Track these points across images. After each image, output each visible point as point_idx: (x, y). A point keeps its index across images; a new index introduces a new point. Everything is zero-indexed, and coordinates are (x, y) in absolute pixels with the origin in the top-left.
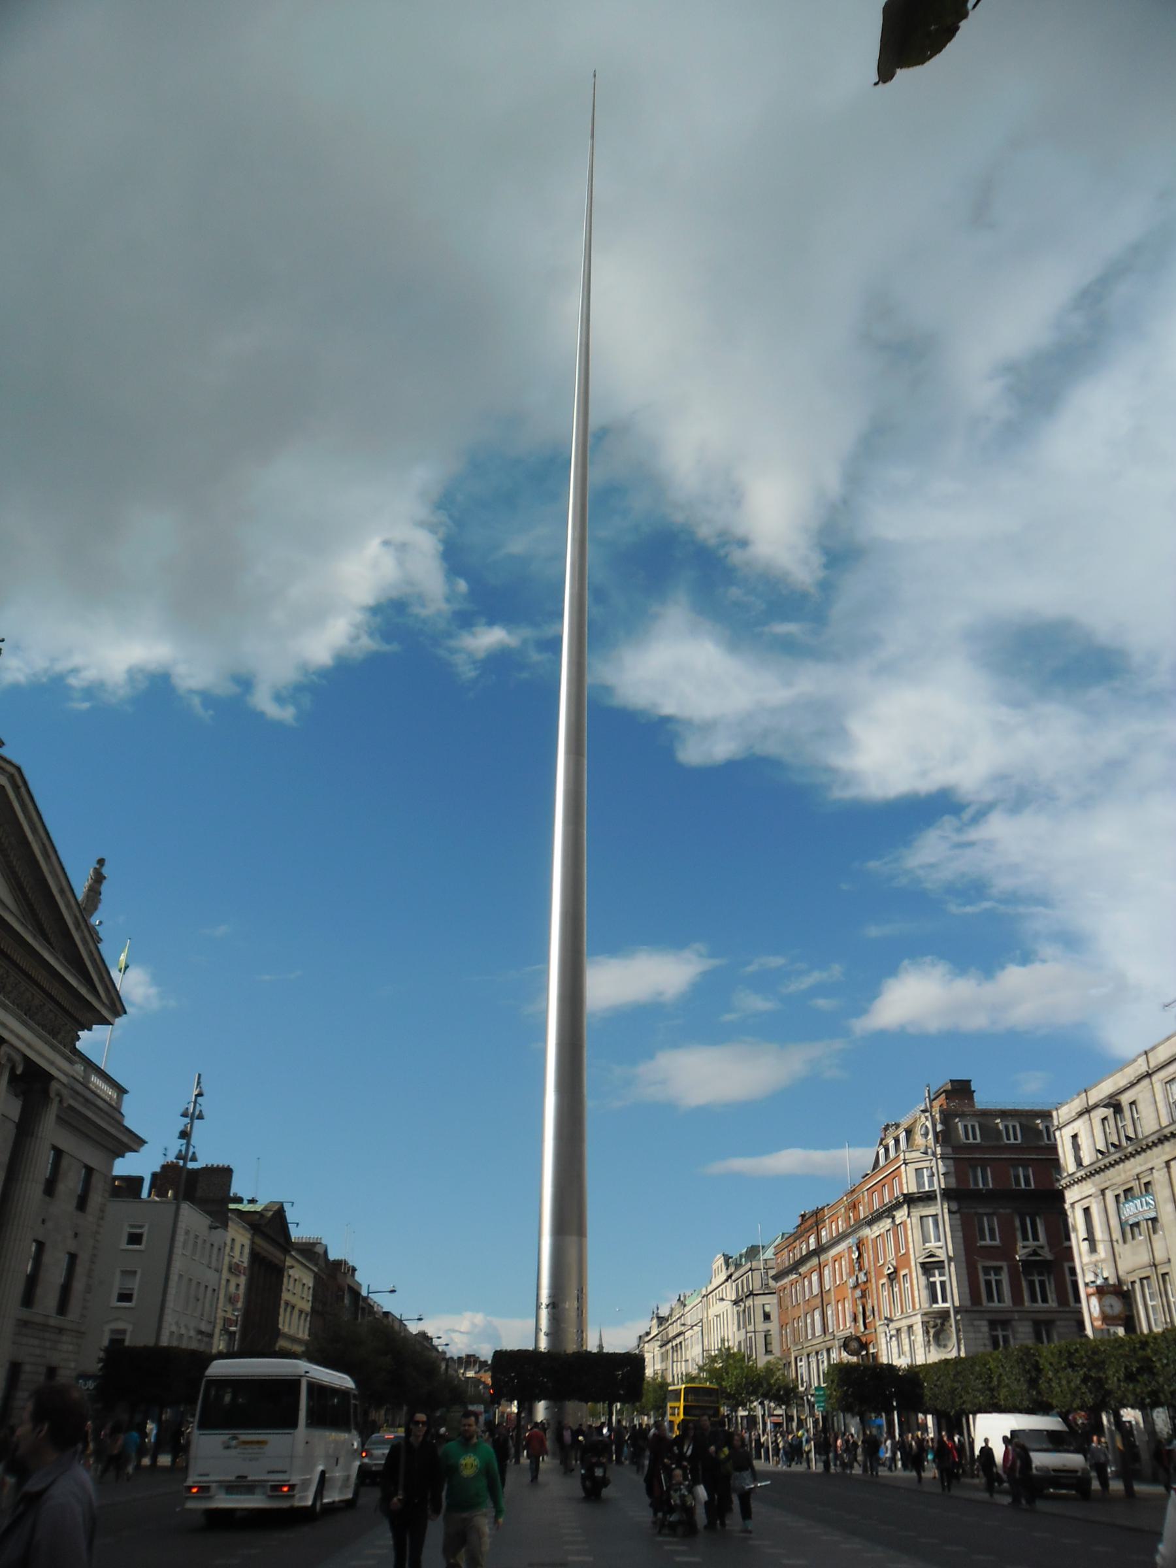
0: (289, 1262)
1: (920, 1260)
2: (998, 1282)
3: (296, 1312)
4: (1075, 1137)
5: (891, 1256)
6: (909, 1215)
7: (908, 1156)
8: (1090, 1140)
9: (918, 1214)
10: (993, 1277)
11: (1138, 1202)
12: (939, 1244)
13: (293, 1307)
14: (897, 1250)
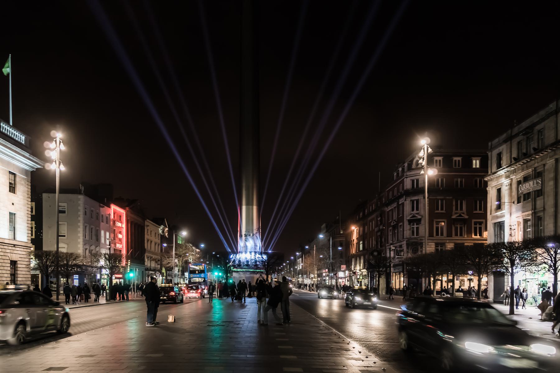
0: (146, 223)
1: (408, 218)
3: (153, 244)
5: (395, 217)
6: (405, 200)
7: (408, 173)
8: (509, 155)
9: (409, 199)
10: (478, 226)
11: (531, 183)
12: (418, 212)
13: (151, 242)
14: (398, 214)
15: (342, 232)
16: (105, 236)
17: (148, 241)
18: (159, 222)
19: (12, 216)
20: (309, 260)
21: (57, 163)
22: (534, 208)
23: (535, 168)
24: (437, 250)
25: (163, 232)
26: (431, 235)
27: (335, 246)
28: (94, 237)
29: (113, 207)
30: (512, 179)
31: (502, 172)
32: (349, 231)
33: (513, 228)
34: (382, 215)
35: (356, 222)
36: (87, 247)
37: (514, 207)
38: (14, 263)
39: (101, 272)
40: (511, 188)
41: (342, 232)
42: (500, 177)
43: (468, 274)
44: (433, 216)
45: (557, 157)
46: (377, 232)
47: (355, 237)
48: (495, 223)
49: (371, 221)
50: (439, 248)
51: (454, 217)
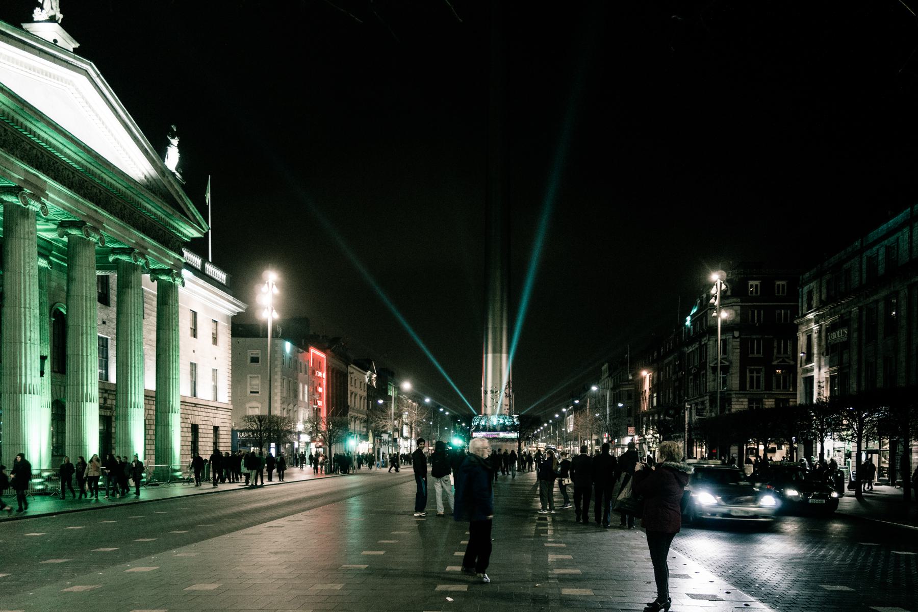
0: (350, 369)
2: (758, 378)
3: (358, 397)
4: (810, 293)
14: (700, 359)
15: (630, 378)
16: (304, 391)
18: (365, 367)
19: (215, 371)
20: (581, 420)
21: (270, 309)
22: (840, 364)
23: (842, 315)
24: (750, 408)
25: (370, 380)
27: (615, 399)
28: (292, 394)
29: (313, 351)
30: (821, 325)
31: (811, 316)
32: (639, 378)
33: (822, 385)
34: (681, 356)
35: (647, 365)
36: (285, 406)
38: (216, 429)
39: (299, 438)
40: (819, 337)
41: (630, 378)
42: (810, 320)
44: (745, 361)
45: (861, 304)
46: (675, 381)
47: (647, 386)
49: (668, 364)
50: (754, 406)
51: (775, 363)
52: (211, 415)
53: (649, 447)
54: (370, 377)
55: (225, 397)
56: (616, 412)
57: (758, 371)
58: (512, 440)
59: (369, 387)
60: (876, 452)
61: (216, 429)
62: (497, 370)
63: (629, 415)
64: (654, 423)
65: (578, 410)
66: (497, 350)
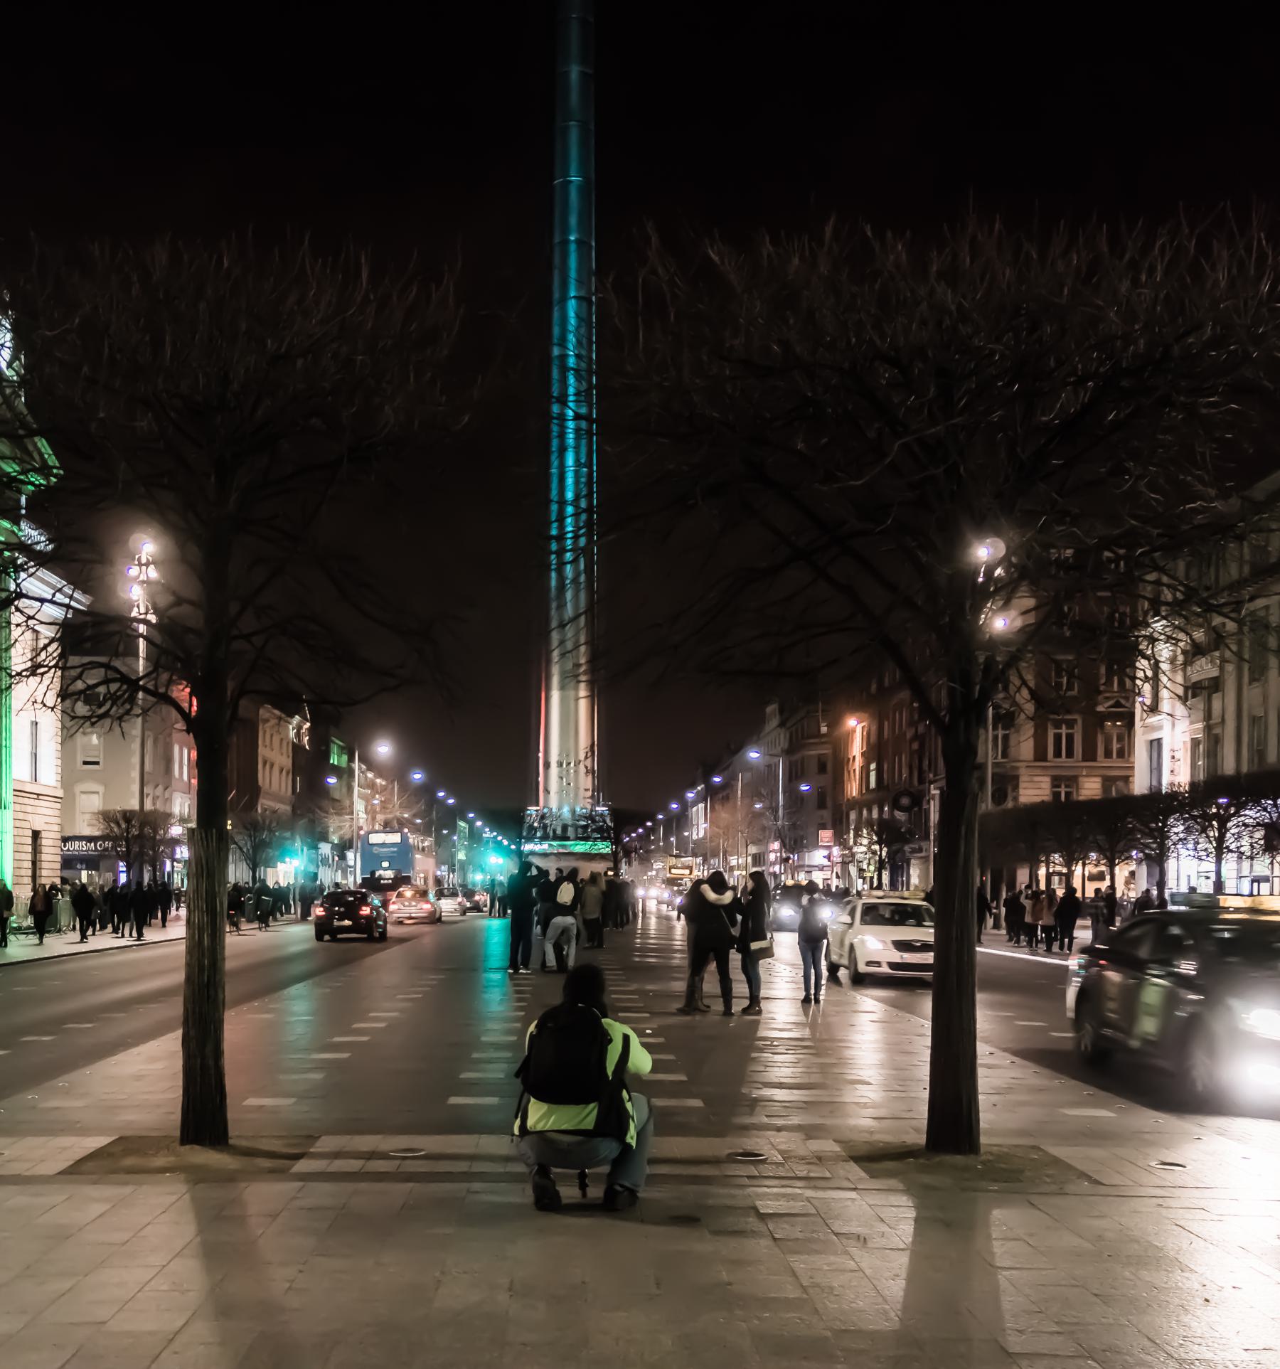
2: (1070, 738)
13: (272, 766)
15: (824, 729)
17: (265, 763)
18: (289, 706)
20: (724, 815)
22: (1208, 716)
24: (1056, 795)
25: (298, 735)
26: (1040, 755)
27: (794, 775)
35: (858, 706)
37: (1180, 710)
38: (36, 835)
39: (173, 852)
43: (1130, 857)
47: (857, 748)
48: (1151, 742)
52: (29, 809)
53: (861, 870)
54: (297, 728)
55: (50, 775)
56: (795, 801)
57: (1071, 724)
58: (602, 857)
59: (297, 748)
60: (1266, 879)
61: (36, 835)
62: (567, 727)
63: (821, 805)
64: (870, 824)
65: (712, 794)
66: (570, 678)
